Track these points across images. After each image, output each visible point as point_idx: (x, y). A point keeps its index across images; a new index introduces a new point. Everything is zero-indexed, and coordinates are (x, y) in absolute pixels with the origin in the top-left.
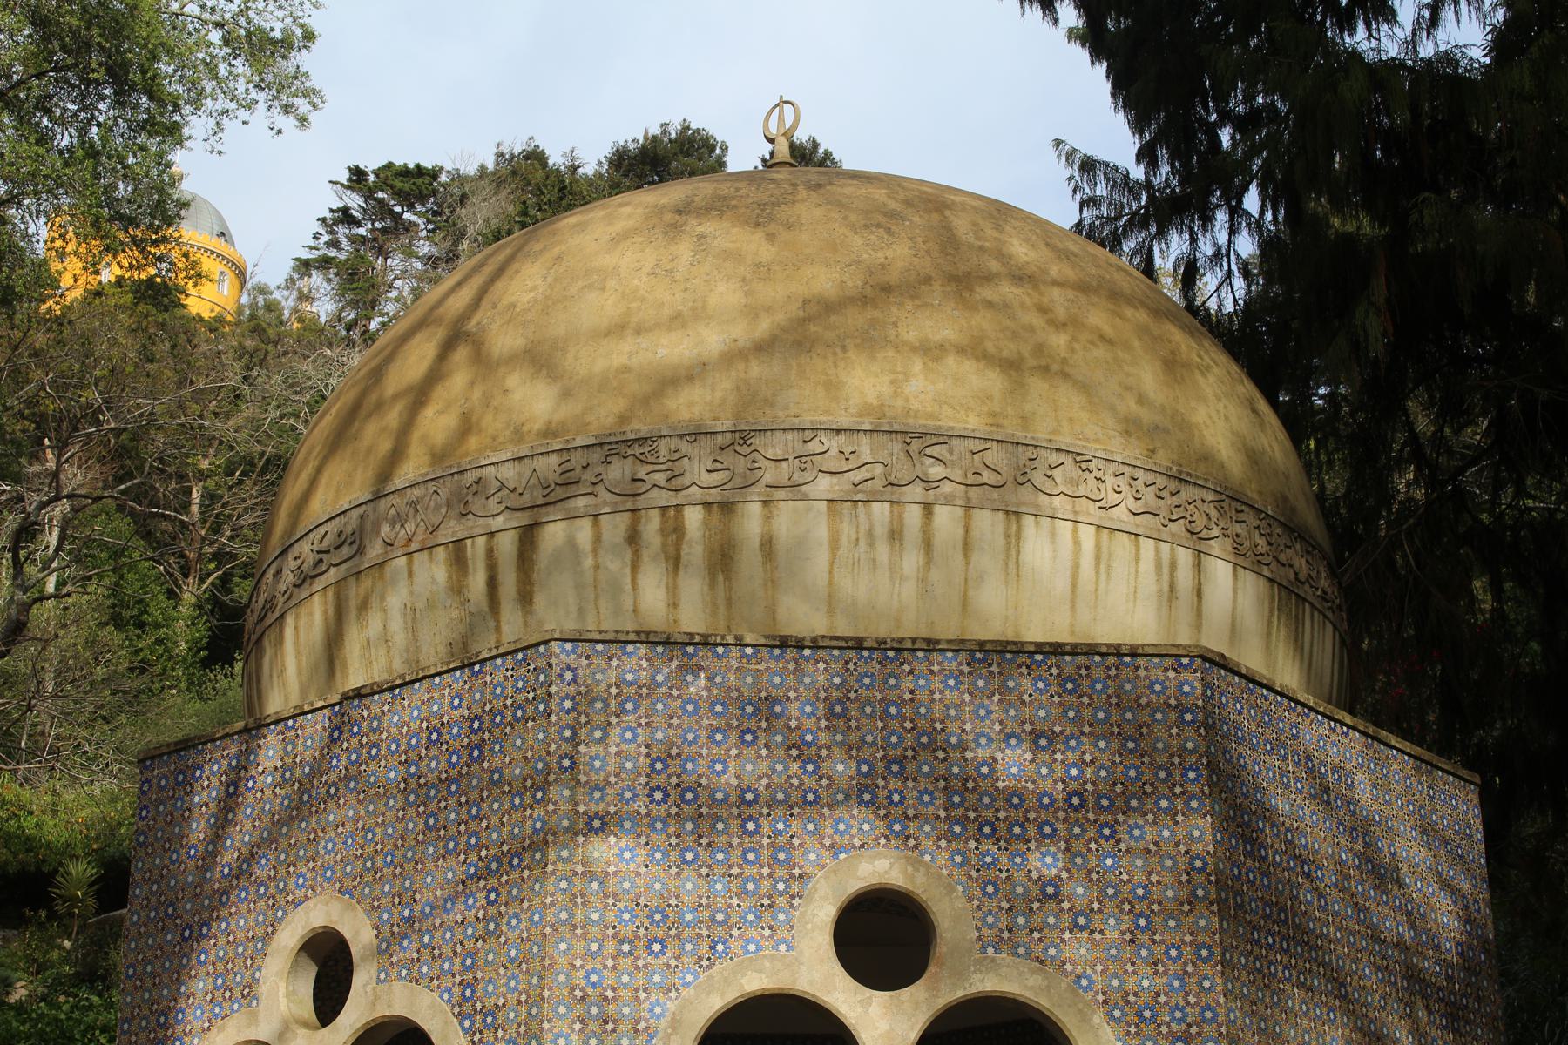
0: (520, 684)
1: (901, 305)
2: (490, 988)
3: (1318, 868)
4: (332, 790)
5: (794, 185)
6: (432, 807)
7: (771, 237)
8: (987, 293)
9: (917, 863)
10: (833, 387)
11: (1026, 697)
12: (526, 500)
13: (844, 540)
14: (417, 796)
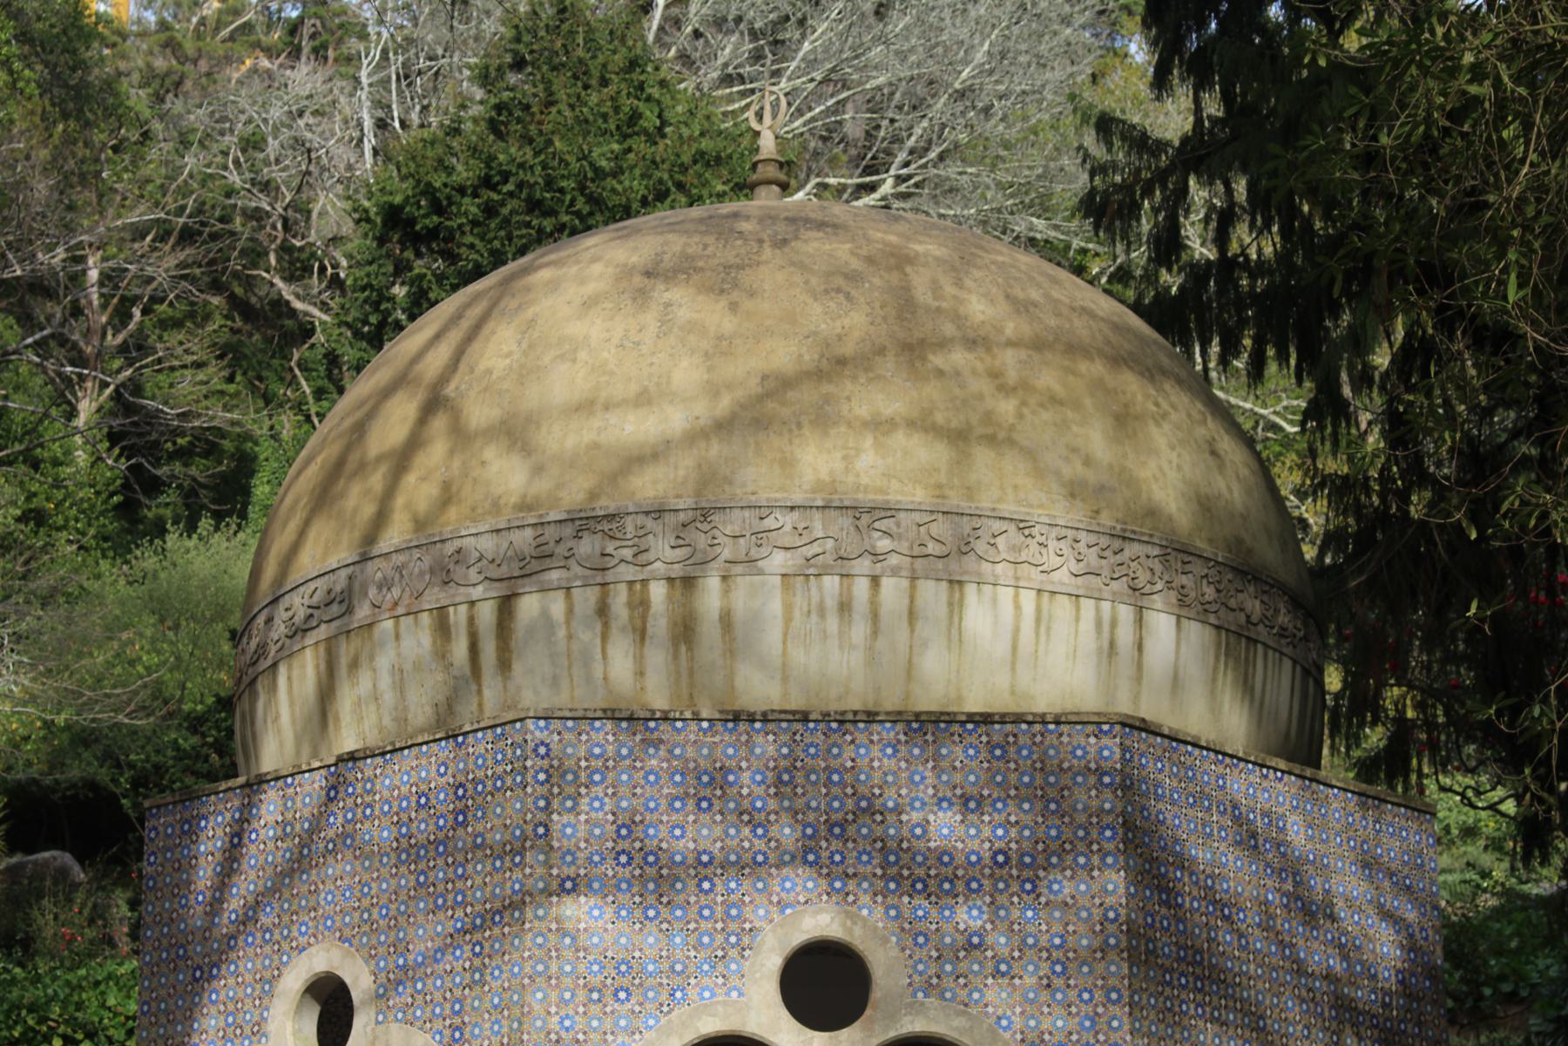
0: (499, 757)
1: (854, 378)
2: (477, 1031)
3: (1240, 910)
4: (331, 846)
5: (761, 241)
6: (422, 866)
7: (734, 307)
8: (937, 360)
9: (854, 918)
10: (787, 464)
11: (958, 764)
12: (504, 571)
13: (797, 613)
14: (409, 855)
